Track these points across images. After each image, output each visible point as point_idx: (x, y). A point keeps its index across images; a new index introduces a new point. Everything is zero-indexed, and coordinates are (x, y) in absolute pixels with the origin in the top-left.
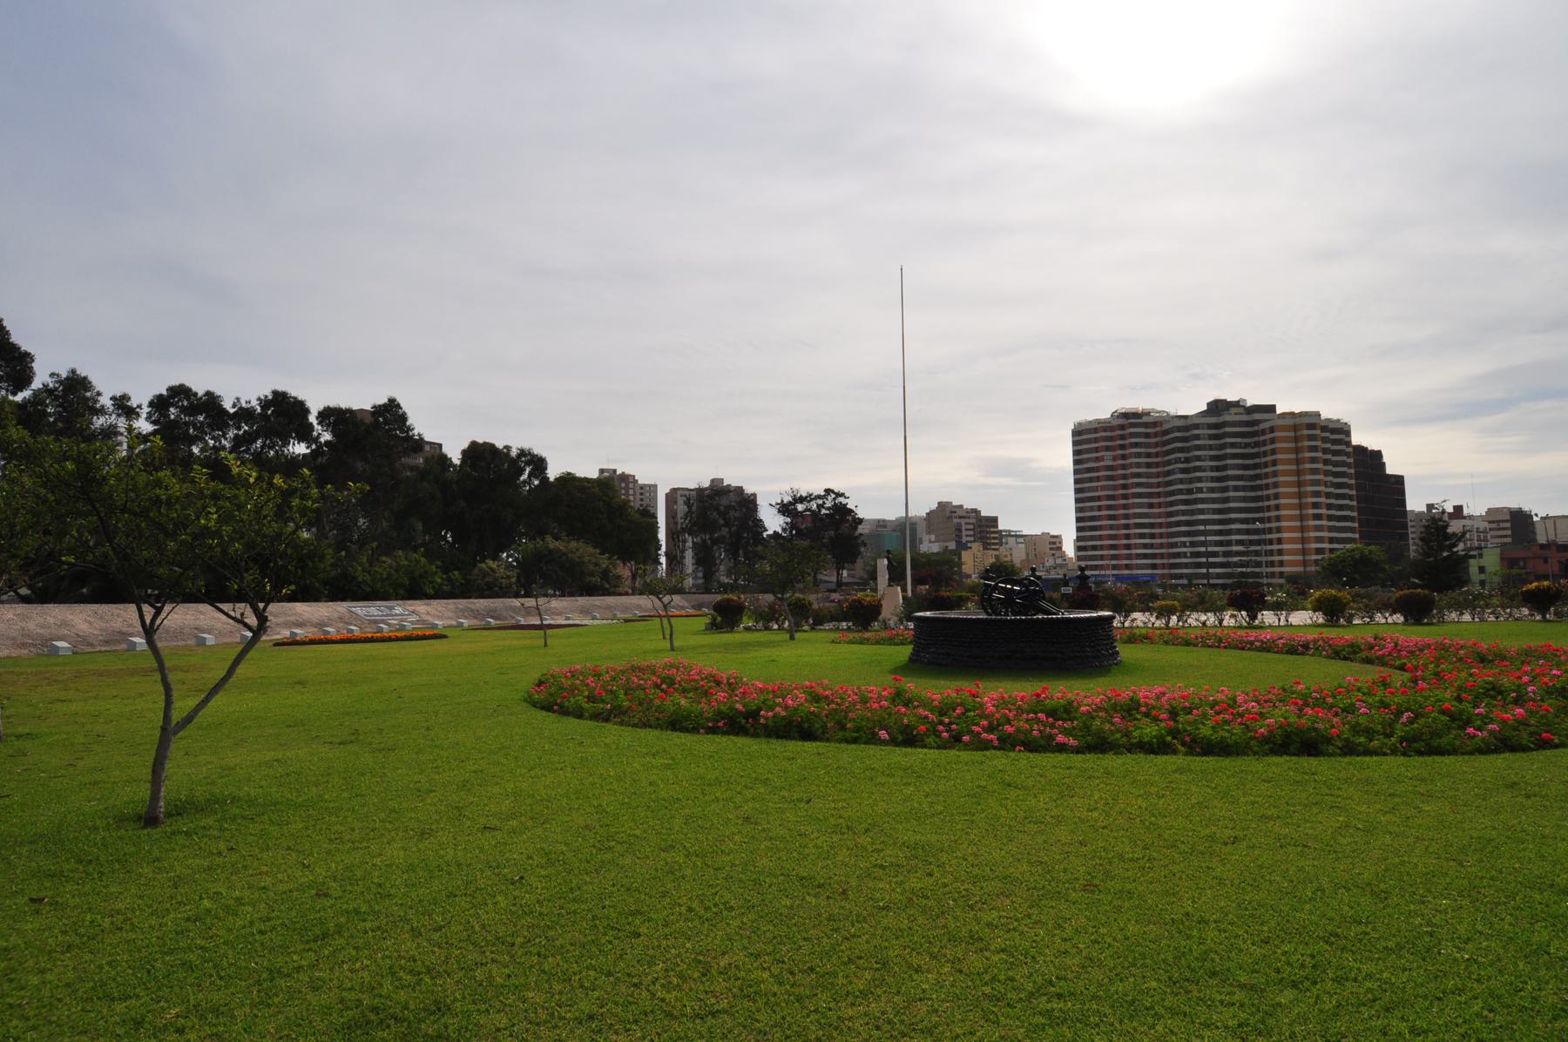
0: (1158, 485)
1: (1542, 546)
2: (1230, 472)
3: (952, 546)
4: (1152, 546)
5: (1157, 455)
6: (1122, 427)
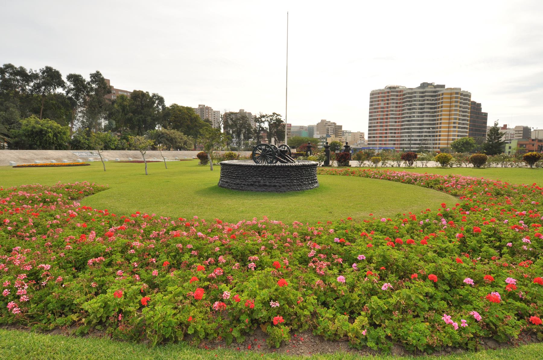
0: (399, 114)
1: (533, 140)
2: (425, 110)
3: (325, 136)
5: (400, 103)
6: (388, 92)
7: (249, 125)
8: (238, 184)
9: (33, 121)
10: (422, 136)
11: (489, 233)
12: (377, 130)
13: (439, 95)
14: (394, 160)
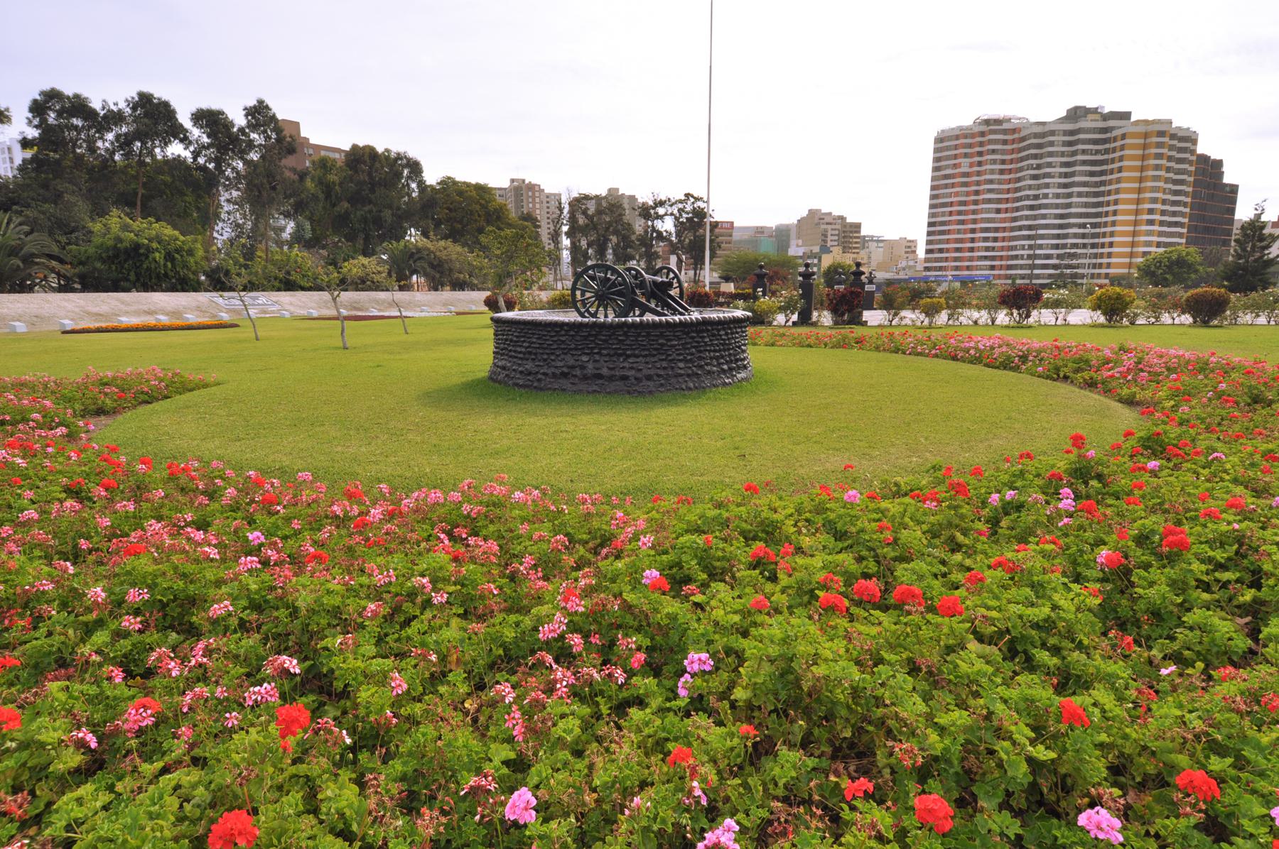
0: (1008, 191)
2: (1077, 179)
3: (816, 249)
4: (993, 249)
5: (1011, 161)
6: (983, 134)
7: (629, 227)
8: (530, 374)
9: (117, 225)
10: (1064, 246)
11: (1220, 555)
12: (949, 232)
13: (1115, 139)
14: (979, 308)
